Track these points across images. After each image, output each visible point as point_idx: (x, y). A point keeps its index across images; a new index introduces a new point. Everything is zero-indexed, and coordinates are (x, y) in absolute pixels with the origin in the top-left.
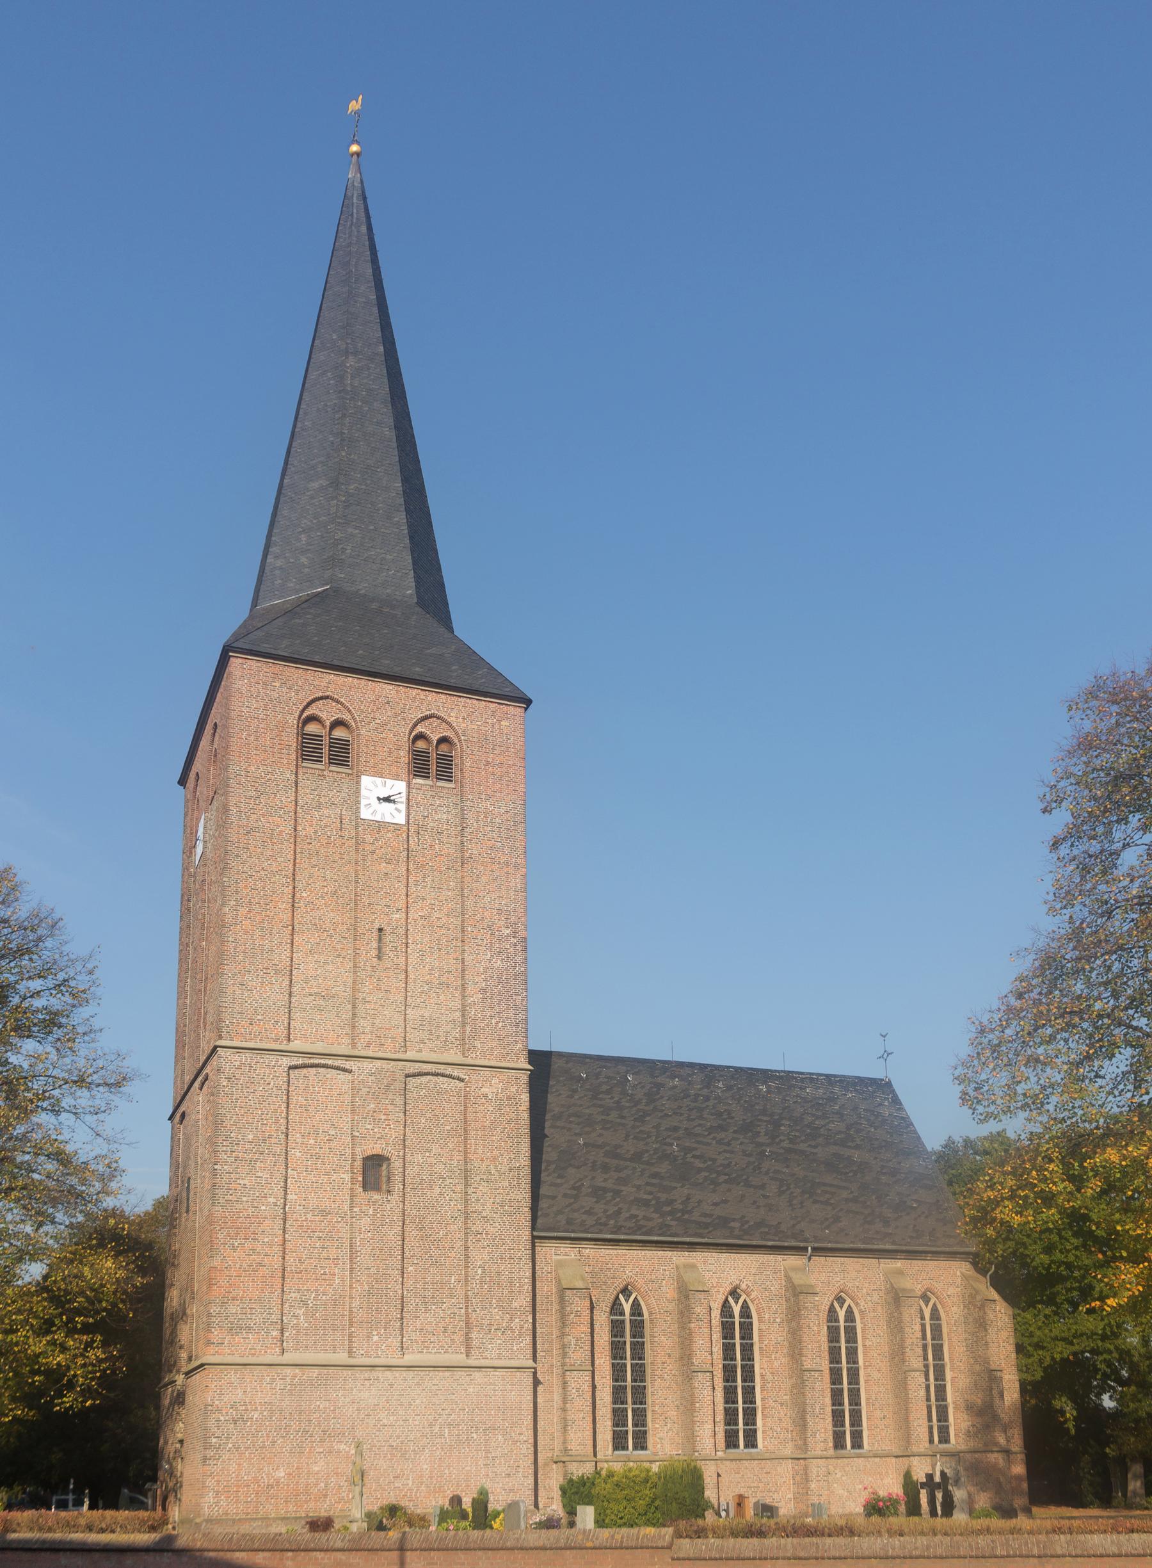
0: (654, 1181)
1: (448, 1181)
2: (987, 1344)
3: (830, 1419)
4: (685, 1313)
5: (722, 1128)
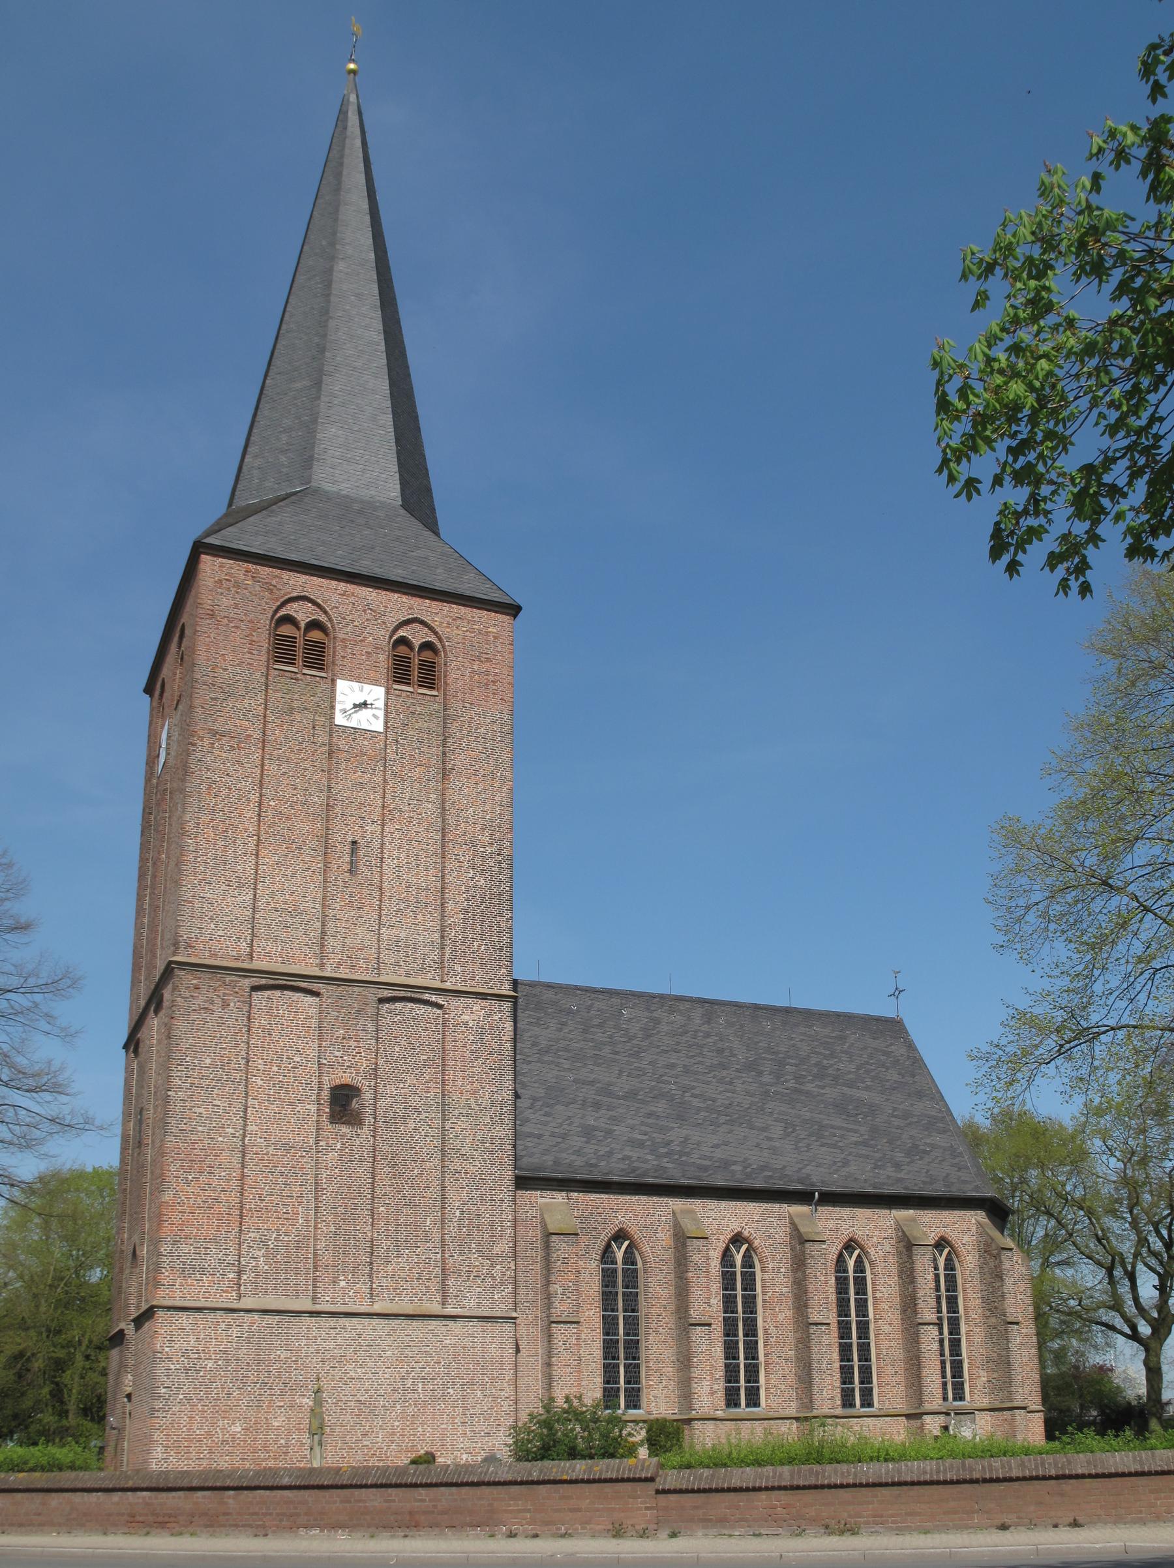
0: (650, 1121)
1: (424, 1115)
2: (1003, 1295)
3: (838, 1376)
4: (681, 1263)
5: (723, 1066)
